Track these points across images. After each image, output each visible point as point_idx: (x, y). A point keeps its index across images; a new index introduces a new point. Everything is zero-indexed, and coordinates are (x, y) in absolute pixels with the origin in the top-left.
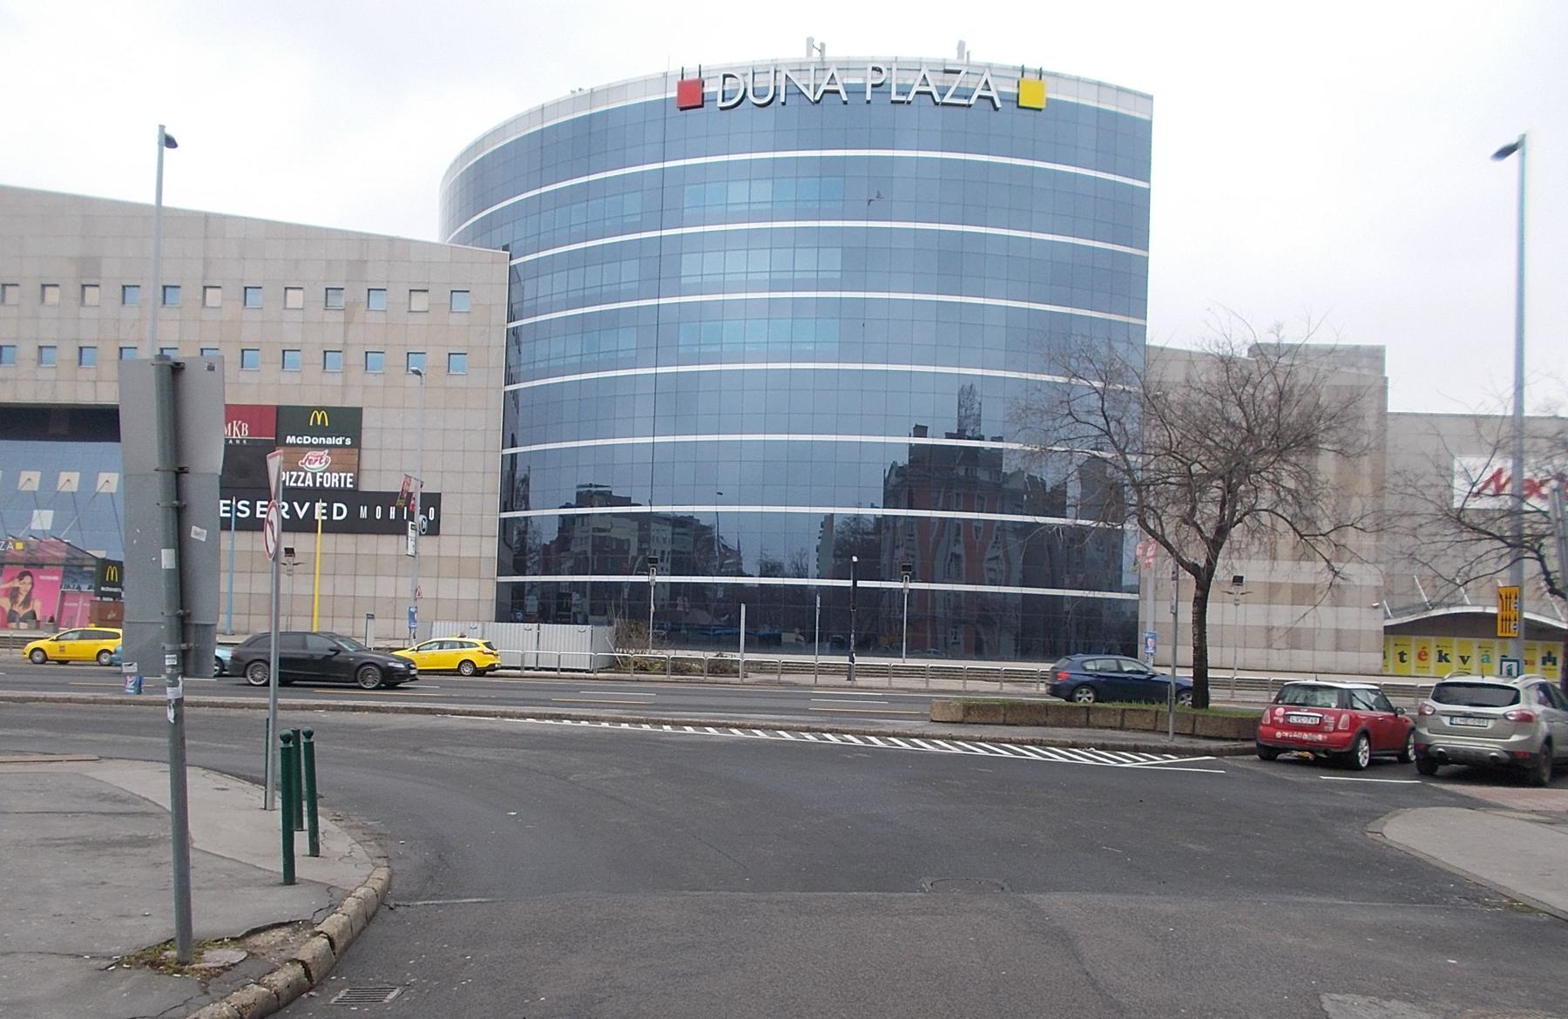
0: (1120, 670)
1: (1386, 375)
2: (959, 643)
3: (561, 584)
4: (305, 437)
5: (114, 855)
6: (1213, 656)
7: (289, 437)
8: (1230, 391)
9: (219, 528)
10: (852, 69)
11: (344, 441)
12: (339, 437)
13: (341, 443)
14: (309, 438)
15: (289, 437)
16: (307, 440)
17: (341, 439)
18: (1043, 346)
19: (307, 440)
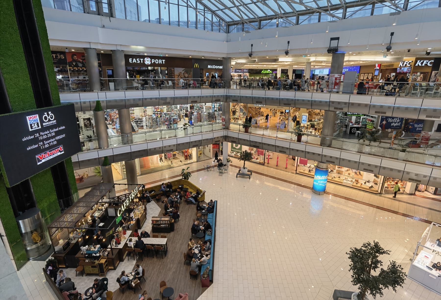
4: (214, 66)
15: (209, 66)
16: (214, 67)
19: (214, 67)
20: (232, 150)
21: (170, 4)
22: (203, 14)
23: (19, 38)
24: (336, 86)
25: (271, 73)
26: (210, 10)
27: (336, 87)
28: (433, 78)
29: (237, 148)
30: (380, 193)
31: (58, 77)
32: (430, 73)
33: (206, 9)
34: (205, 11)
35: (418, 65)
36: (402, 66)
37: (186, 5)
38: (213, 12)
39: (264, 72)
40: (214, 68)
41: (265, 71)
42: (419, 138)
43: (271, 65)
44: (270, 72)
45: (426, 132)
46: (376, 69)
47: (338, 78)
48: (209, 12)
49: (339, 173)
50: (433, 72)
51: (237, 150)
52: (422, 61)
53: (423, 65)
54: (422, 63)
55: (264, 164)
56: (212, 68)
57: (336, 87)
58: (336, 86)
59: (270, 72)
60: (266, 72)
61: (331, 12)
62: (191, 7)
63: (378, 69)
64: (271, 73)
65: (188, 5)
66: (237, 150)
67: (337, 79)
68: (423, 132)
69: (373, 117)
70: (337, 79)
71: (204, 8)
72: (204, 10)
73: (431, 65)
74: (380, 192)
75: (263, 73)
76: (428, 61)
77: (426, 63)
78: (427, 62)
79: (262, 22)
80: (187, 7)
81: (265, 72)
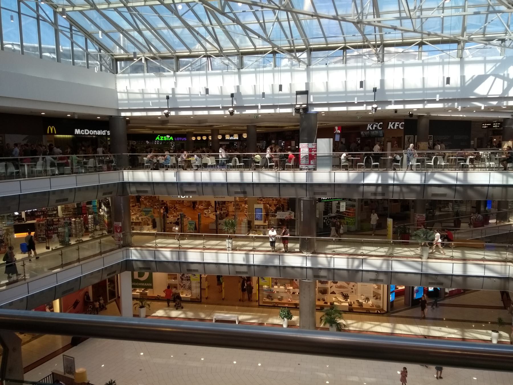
0: (199, 156)
1: (465, 74)
2: (181, 214)
3: (113, 117)
4: (86, 130)
5: (411, 332)
6: (265, 19)
7: (76, 130)
8: (447, 60)
9: (328, 331)
10: (85, 259)
11: (106, 133)
12: (104, 130)
13: (105, 134)
14: (88, 130)
15: (76, 130)
16: (87, 132)
17: (105, 131)
18: (237, 205)
19: (87, 132)
20: (133, 286)
21: (22, 16)
22: (69, 35)
23: (41, 109)
24: (311, 161)
25: (172, 139)
26: (81, 29)
27: (312, 162)
28: (407, 144)
29: (142, 279)
30: (387, 312)
31: (438, 234)
32: (403, 137)
33: (73, 28)
34: (73, 32)
35: (390, 127)
36: (371, 129)
37: (35, 15)
38: (88, 36)
39: (160, 138)
40: (86, 134)
41: (162, 137)
42: (241, 209)
43: (170, 126)
44: (169, 138)
45: (421, 214)
46: (337, 133)
47: (312, 148)
48: (79, 33)
49: (376, 296)
50: (406, 136)
51: (143, 284)
52: (393, 123)
53: (395, 128)
54: (394, 126)
55: (201, 302)
56: (83, 134)
57: (312, 162)
58: (311, 161)
59: (169, 138)
60: (163, 138)
61: (297, 53)
62: (45, 20)
63: (339, 133)
64: (172, 139)
65: (38, 16)
66: (143, 284)
67: (312, 150)
68: (417, 214)
69: (351, 201)
70: (312, 150)
71: (71, 26)
72: (71, 29)
73: (403, 128)
74: (386, 310)
75: (158, 140)
76: (399, 123)
77: (398, 125)
78: (398, 124)
79: (180, 59)
80: (38, 19)
81: (161, 139)
